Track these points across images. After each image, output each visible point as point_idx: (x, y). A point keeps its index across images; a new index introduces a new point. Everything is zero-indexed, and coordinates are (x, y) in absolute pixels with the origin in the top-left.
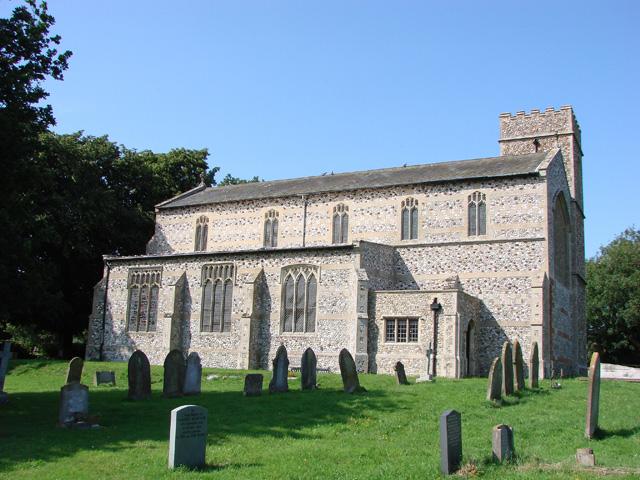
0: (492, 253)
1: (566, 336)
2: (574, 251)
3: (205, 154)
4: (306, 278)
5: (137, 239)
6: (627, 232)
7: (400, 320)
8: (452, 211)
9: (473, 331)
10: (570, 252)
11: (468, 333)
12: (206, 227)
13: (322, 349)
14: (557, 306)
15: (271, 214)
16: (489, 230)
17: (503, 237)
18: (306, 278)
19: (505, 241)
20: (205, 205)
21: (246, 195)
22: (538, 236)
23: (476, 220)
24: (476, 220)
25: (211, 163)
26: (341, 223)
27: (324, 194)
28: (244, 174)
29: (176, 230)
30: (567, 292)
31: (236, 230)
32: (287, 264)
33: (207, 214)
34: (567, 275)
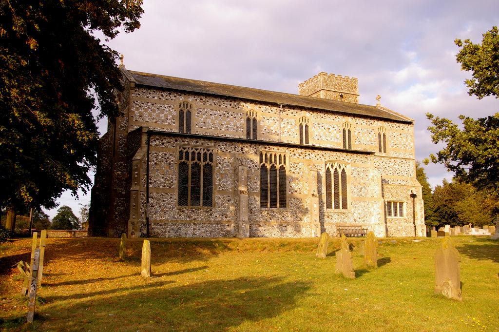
0: (391, 164)
8: (370, 136)
12: (189, 113)
15: (346, 124)
26: (185, 116)
32: (328, 159)
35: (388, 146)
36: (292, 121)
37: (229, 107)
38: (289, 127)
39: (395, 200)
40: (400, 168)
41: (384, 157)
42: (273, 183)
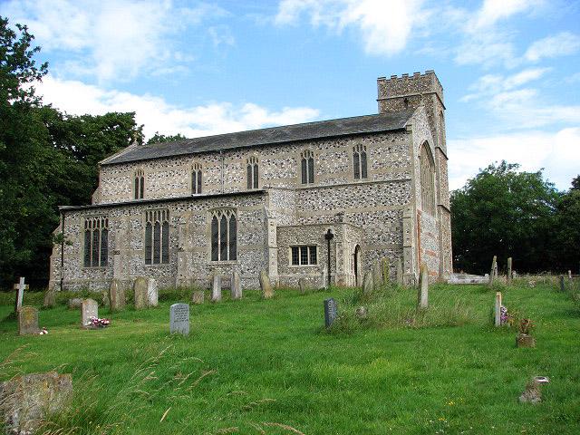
1: (433, 254)
2: (438, 187)
3: (133, 114)
4: (228, 218)
5: (79, 194)
6: (490, 168)
7: (304, 249)
9: (359, 254)
10: (435, 187)
11: (355, 256)
12: (142, 179)
13: (242, 273)
14: (424, 231)
16: (369, 175)
17: (379, 180)
18: (228, 218)
19: (383, 182)
20: (140, 161)
21: (173, 150)
22: (407, 177)
23: (360, 168)
24: (360, 168)
25: (138, 120)
27: (238, 149)
28: (169, 131)
29: (114, 187)
30: (434, 220)
31: (167, 182)
32: (211, 207)
33: (142, 167)
34: (433, 207)
35: (370, 169)
36: (238, 165)
37: (175, 165)
38: (234, 172)
39: (301, 244)
40: (387, 194)
41: (361, 185)
42: (157, 240)
